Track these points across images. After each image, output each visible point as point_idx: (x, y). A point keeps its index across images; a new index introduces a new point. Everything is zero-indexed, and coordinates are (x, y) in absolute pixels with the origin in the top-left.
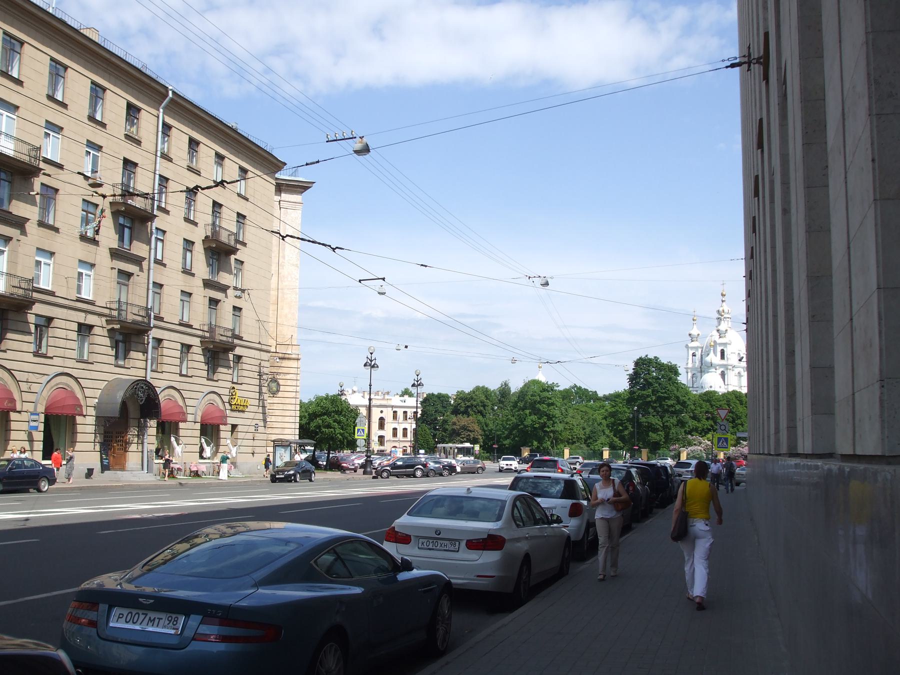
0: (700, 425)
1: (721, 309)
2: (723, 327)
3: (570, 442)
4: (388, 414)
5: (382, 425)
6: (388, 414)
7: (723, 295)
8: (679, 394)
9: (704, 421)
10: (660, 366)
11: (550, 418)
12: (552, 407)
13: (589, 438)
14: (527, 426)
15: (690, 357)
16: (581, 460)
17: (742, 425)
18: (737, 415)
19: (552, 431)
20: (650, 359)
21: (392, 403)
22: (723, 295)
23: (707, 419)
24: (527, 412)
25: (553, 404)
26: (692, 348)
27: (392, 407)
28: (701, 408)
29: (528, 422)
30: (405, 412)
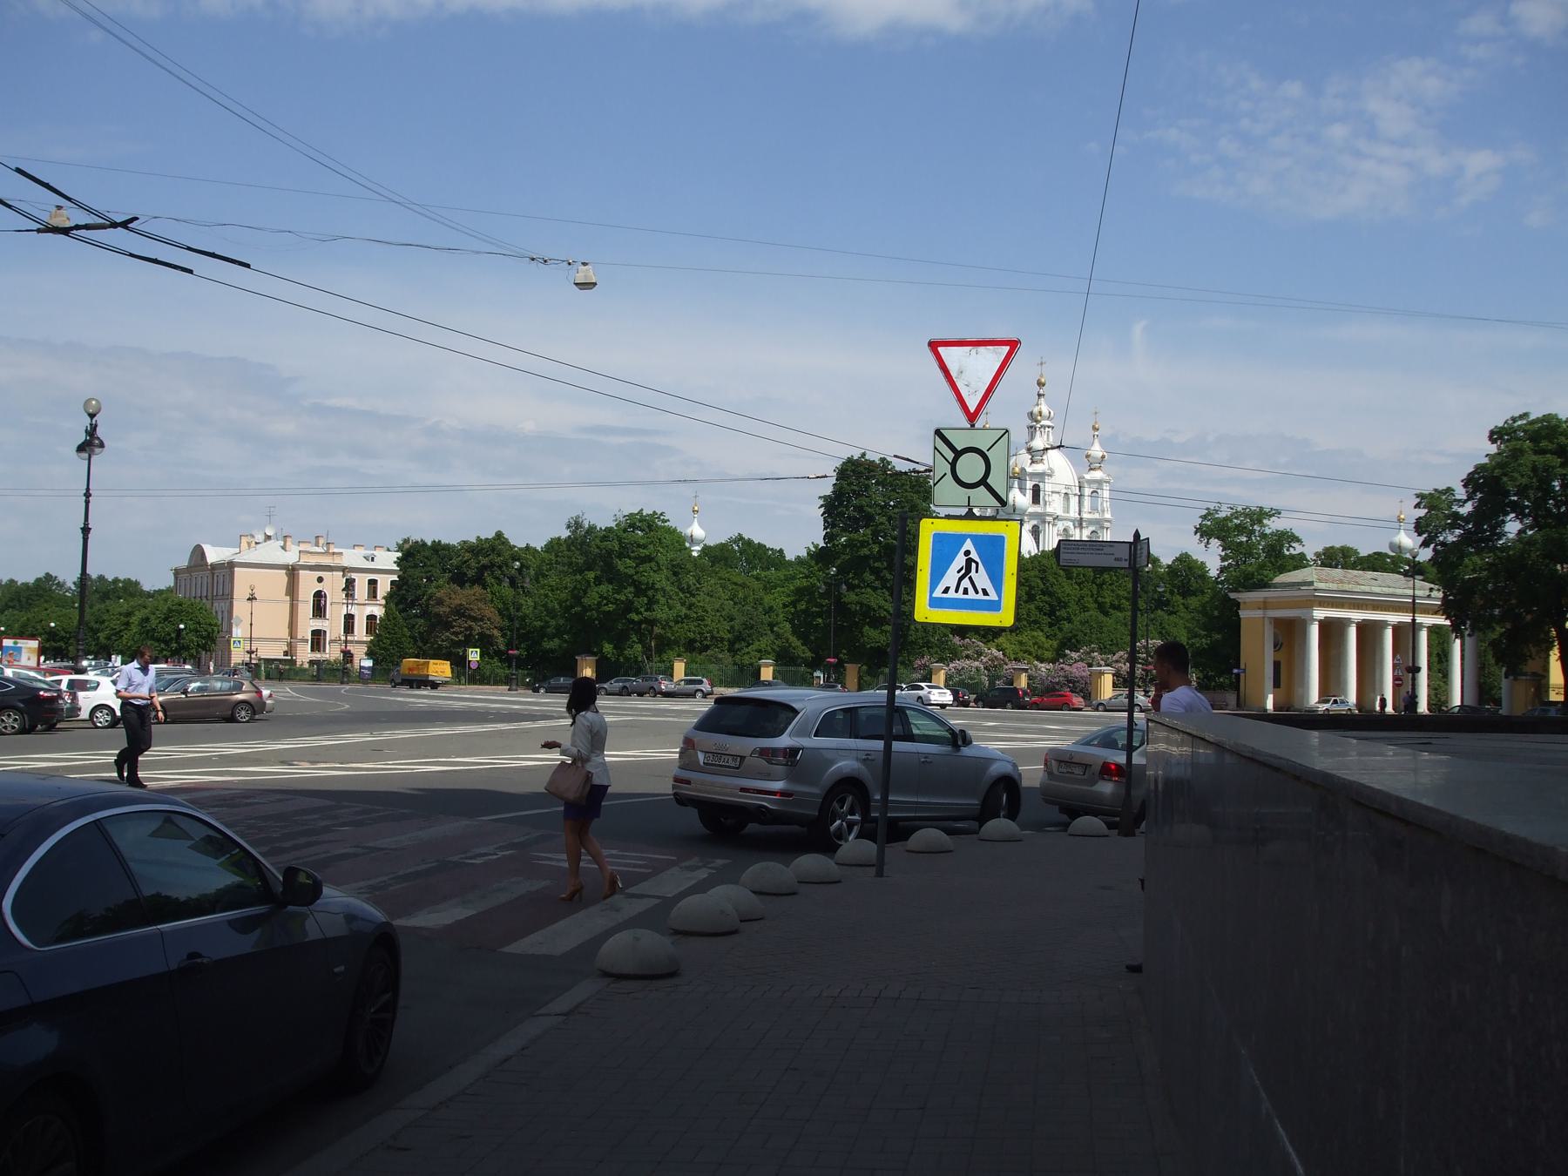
1: (1036, 410)
3: (691, 647)
5: (319, 610)
6: (333, 586)
11: (640, 590)
12: (647, 566)
13: (739, 638)
14: (589, 609)
16: (706, 687)
17: (1069, 620)
18: (1059, 601)
19: (646, 621)
24: (591, 575)
25: (649, 559)
27: (344, 570)
29: (592, 598)
30: (373, 583)
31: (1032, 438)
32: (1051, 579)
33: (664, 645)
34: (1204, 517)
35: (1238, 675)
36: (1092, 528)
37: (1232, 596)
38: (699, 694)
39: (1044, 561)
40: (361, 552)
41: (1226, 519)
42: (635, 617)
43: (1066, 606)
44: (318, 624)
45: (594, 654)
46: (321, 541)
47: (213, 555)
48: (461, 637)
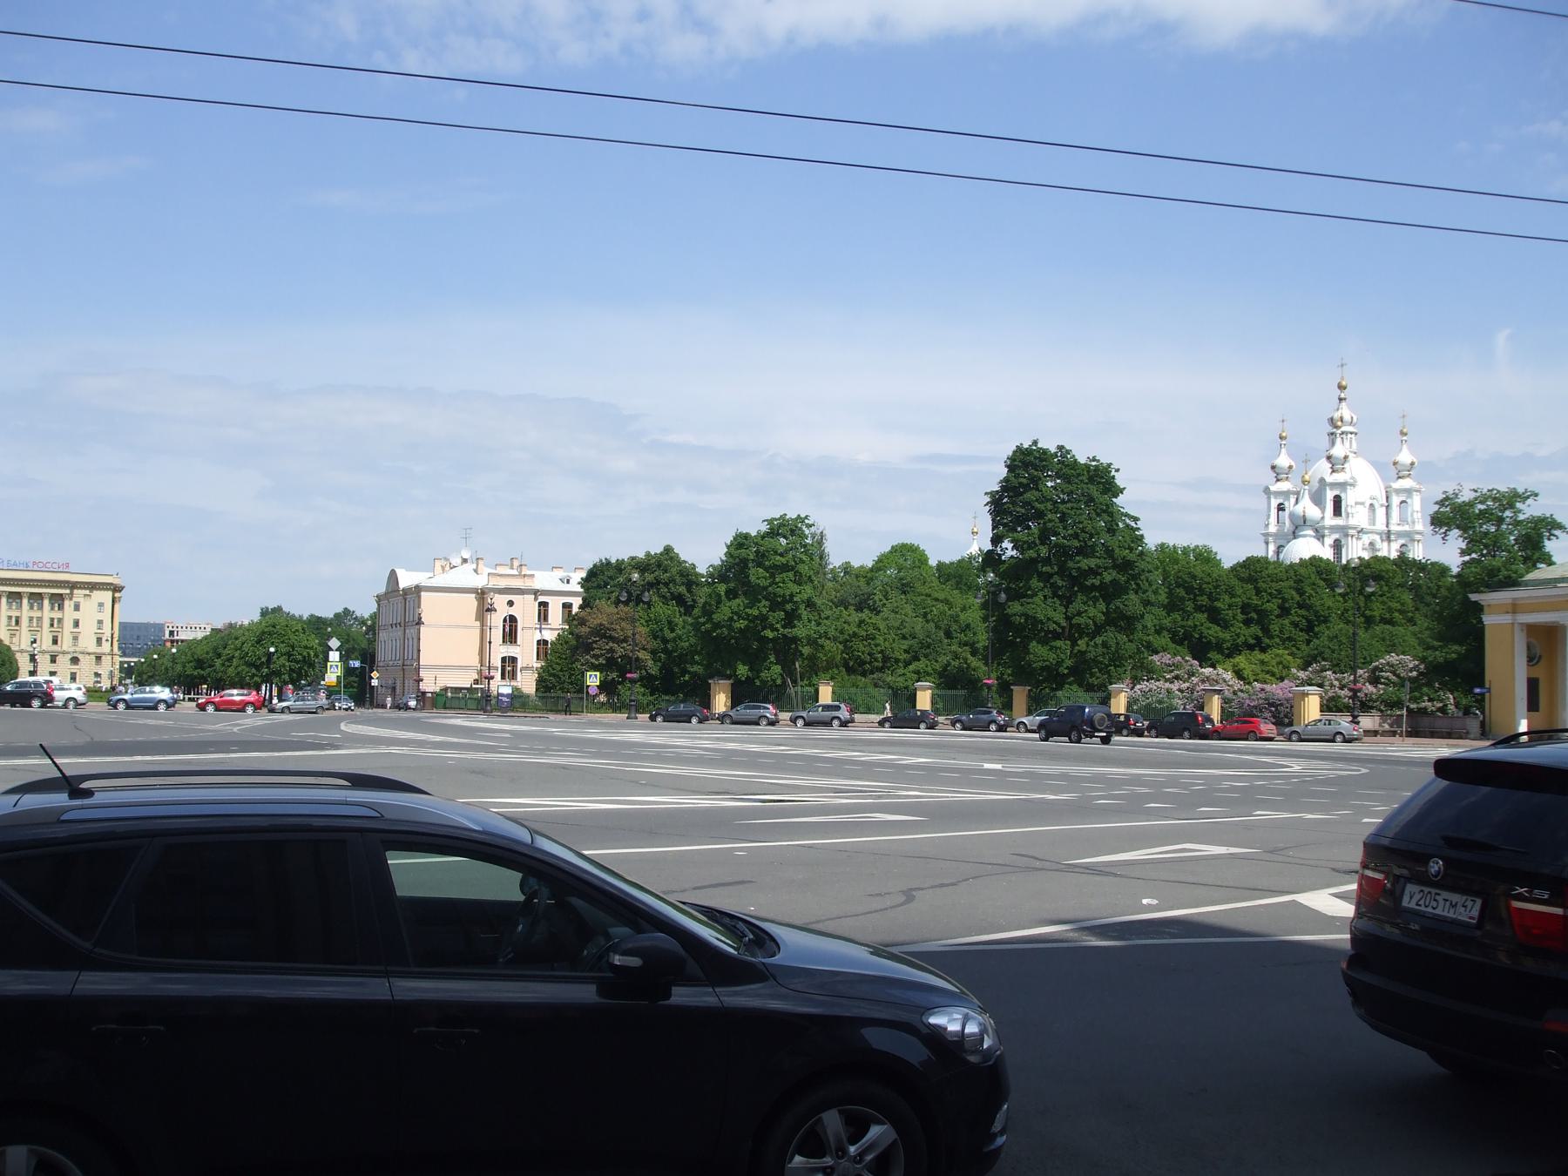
0: (1227, 636)
1: (1337, 415)
2: (1339, 451)
4: (525, 611)
5: (510, 636)
6: (525, 611)
7: (1341, 387)
8: (1113, 542)
9: (1238, 627)
10: (1065, 466)
15: (1274, 512)
20: (1045, 452)
21: (537, 584)
22: (1341, 387)
23: (1247, 622)
26: (1278, 494)
27: (536, 593)
28: (1232, 596)
29: (724, 613)
31: (1333, 444)
32: (1309, 590)
33: (815, 669)
34: (1441, 503)
35: (1482, 695)
36: (1402, 541)
37: (1473, 597)
38: (836, 723)
39: (1302, 571)
40: (561, 574)
41: (1471, 504)
42: (769, 634)
43: (1326, 620)
44: (510, 651)
45: (728, 677)
46: (516, 563)
47: (406, 580)
48: (602, 661)
